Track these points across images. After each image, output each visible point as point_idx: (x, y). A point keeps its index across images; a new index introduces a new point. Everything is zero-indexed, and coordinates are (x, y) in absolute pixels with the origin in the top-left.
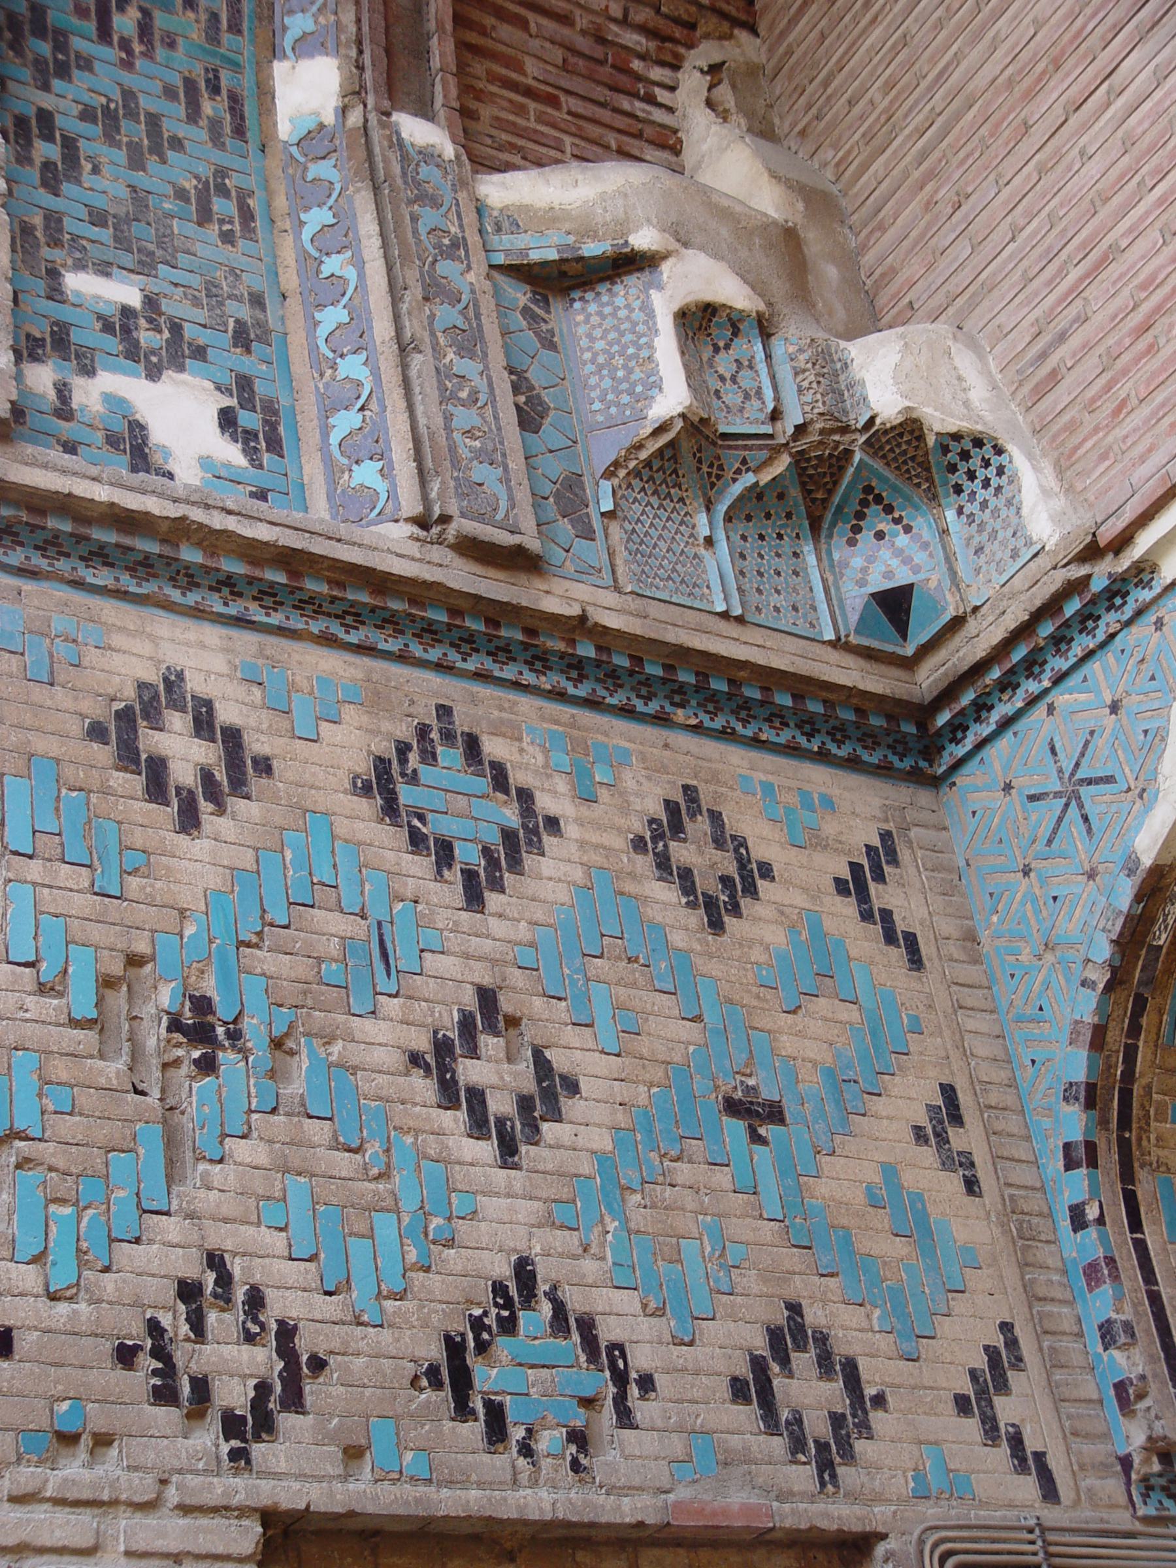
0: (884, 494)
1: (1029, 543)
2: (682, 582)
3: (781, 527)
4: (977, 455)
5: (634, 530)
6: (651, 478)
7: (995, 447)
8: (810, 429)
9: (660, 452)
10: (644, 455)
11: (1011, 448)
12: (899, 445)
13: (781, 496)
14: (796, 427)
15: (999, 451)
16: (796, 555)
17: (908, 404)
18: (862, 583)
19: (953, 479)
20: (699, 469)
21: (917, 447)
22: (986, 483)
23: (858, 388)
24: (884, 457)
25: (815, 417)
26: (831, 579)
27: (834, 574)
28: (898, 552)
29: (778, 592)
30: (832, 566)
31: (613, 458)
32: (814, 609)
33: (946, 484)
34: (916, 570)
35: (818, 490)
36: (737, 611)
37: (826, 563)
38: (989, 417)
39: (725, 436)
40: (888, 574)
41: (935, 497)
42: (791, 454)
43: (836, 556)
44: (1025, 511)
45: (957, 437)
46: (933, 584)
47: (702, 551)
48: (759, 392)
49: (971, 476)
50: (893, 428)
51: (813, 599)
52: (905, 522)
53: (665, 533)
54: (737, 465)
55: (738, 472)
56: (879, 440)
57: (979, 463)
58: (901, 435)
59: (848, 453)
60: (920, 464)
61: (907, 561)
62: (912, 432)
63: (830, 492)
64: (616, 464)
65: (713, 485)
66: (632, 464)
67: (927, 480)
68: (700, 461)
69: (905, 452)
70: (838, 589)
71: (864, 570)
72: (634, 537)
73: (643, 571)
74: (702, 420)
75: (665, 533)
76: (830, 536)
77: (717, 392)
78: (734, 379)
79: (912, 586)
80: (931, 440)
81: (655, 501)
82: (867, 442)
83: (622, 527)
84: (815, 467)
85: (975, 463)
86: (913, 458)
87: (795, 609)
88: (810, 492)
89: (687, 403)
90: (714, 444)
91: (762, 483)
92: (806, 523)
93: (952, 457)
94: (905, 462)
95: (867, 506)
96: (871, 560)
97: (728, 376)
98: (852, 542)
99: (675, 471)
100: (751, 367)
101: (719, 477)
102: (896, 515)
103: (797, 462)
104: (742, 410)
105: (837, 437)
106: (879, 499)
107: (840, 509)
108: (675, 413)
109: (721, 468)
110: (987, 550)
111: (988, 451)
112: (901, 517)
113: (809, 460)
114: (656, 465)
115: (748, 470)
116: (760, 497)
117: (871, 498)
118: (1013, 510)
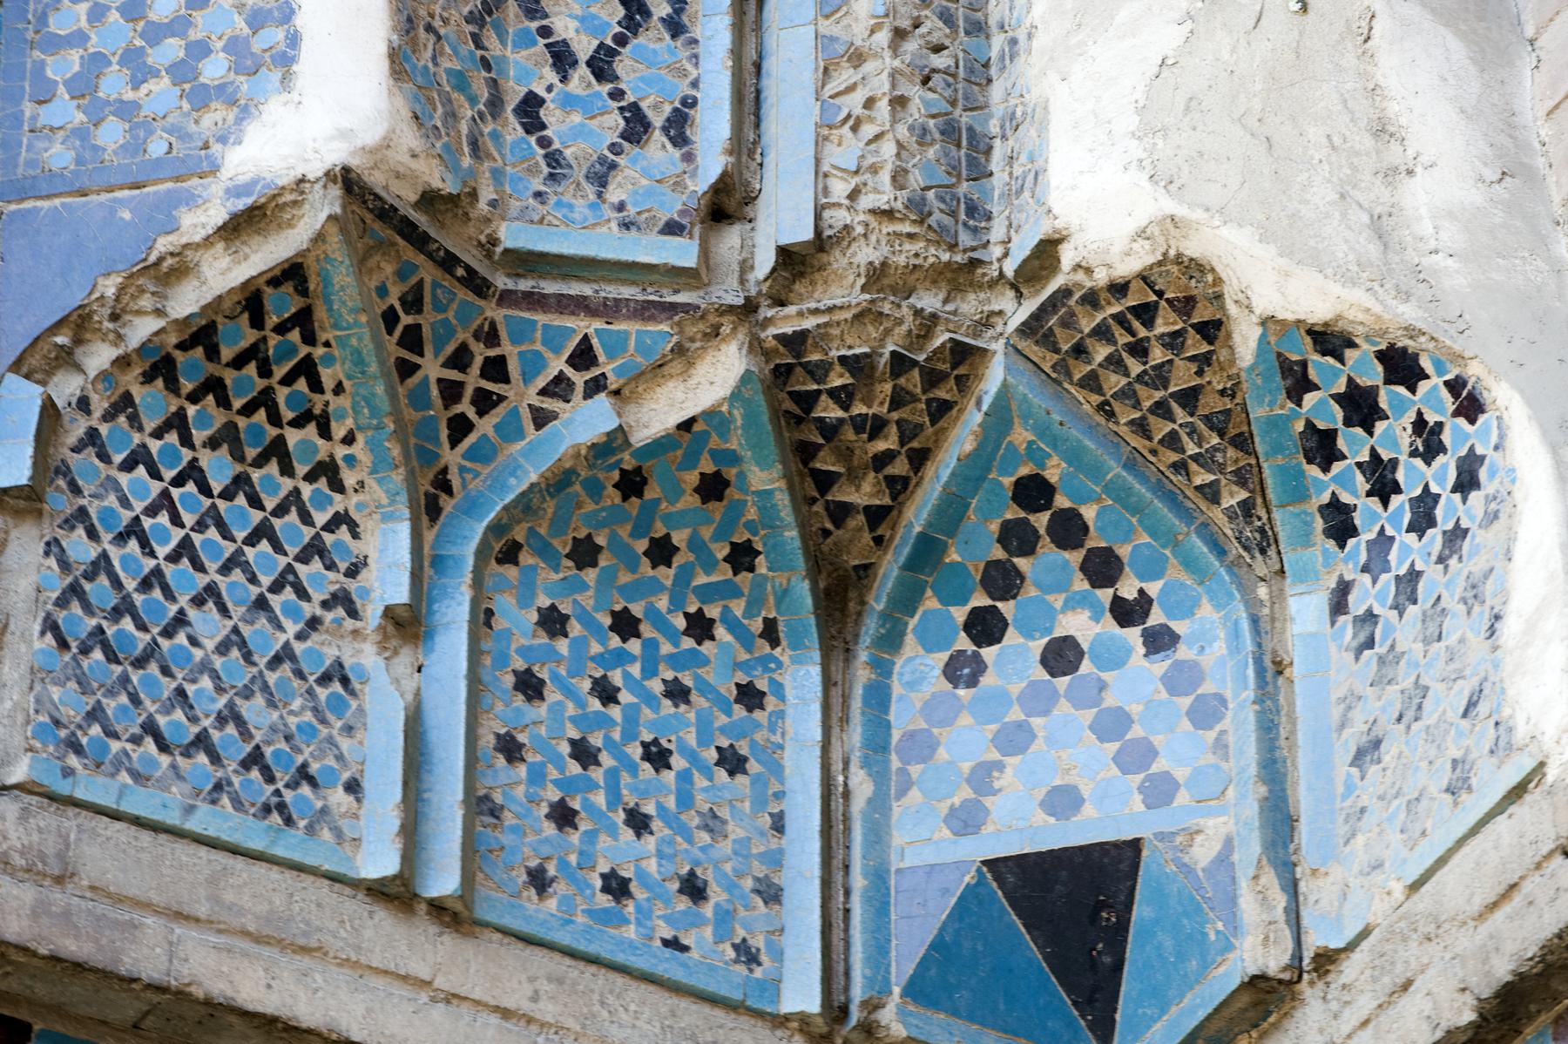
0: (1089, 513)
1: (1502, 747)
2: (254, 759)
3: (707, 593)
4: (1401, 408)
5: (102, 564)
6: (214, 387)
7: (1455, 386)
8: (837, 260)
9: (251, 301)
10: (187, 301)
11: (1501, 395)
12: (1139, 350)
13: (713, 487)
14: (786, 255)
15: (1471, 407)
16: (750, 696)
17: (1169, 206)
18: (966, 821)
19: (1324, 484)
20: (406, 369)
21: (1204, 361)
22: (1423, 519)
23: (1028, 132)
24: (1091, 383)
25: (857, 220)
26: (862, 785)
27: (880, 776)
28: (1112, 725)
29: (639, 822)
30: (878, 743)
31: (75, 298)
32: (771, 894)
33: (1299, 494)
34: (1160, 792)
35: (854, 477)
36: (443, 881)
37: (855, 736)
38: (1454, 277)
39: (527, 262)
40: (1063, 801)
41: (1266, 542)
42: (755, 346)
43: (903, 717)
44: (1510, 629)
45: (1330, 340)
46: (1203, 853)
47: (365, 657)
48: (679, 127)
49: (1383, 485)
50: (1119, 289)
51: (776, 859)
52: (1156, 617)
53: (232, 585)
54: (557, 365)
55: (559, 388)
56: (1068, 323)
57: (1405, 439)
58: (1146, 313)
59: (965, 356)
60: (1216, 425)
61: (1136, 757)
62: (1186, 305)
63: (900, 488)
64: (80, 323)
65: (460, 428)
66: (141, 329)
67: (1241, 479)
68: (412, 340)
69: (1160, 376)
70: (878, 835)
71: (983, 777)
72: (100, 589)
73: (96, 714)
74: (430, 199)
75: (232, 585)
76: (891, 640)
77: (530, 108)
78: (601, 66)
79: (1135, 845)
80: (1245, 341)
81: (219, 468)
82: (1029, 328)
83: (53, 547)
84: (843, 397)
85: (1394, 436)
86: (1189, 398)
87: (694, 889)
88: (825, 481)
89: (371, 135)
90: (478, 285)
91: (641, 436)
92: (803, 591)
93: (1320, 407)
94: (1161, 409)
95: (1028, 549)
96: (1015, 739)
97: (584, 47)
98: (963, 671)
99: (307, 370)
100: (675, 27)
101: (485, 403)
102: (1128, 589)
103: (782, 374)
104: (601, 176)
105: (929, 301)
106: (1069, 530)
107: (927, 552)
108: (315, 170)
109: (496, 369)
110: (1389, 753)
111: (1432, 399)
112: (1144, 601)
113: (818, 371)
114: (238, 336)
115: (595, 386)
116: (632, 484)
117: (1041, 520)
118: (1482, 614)
